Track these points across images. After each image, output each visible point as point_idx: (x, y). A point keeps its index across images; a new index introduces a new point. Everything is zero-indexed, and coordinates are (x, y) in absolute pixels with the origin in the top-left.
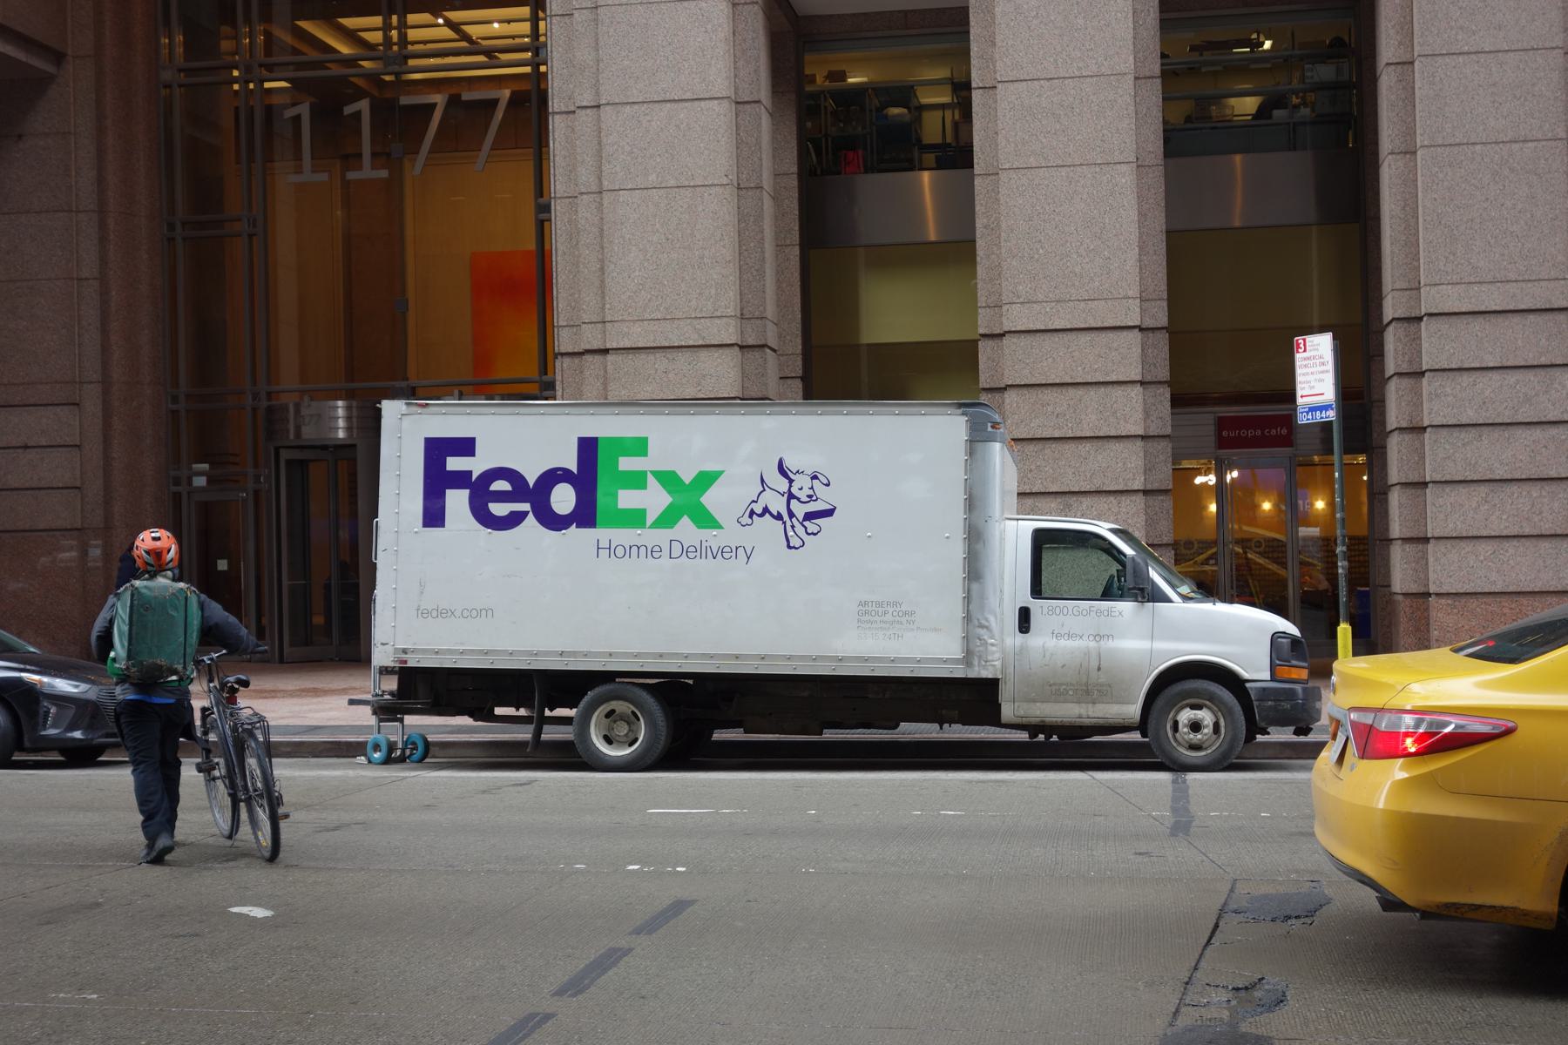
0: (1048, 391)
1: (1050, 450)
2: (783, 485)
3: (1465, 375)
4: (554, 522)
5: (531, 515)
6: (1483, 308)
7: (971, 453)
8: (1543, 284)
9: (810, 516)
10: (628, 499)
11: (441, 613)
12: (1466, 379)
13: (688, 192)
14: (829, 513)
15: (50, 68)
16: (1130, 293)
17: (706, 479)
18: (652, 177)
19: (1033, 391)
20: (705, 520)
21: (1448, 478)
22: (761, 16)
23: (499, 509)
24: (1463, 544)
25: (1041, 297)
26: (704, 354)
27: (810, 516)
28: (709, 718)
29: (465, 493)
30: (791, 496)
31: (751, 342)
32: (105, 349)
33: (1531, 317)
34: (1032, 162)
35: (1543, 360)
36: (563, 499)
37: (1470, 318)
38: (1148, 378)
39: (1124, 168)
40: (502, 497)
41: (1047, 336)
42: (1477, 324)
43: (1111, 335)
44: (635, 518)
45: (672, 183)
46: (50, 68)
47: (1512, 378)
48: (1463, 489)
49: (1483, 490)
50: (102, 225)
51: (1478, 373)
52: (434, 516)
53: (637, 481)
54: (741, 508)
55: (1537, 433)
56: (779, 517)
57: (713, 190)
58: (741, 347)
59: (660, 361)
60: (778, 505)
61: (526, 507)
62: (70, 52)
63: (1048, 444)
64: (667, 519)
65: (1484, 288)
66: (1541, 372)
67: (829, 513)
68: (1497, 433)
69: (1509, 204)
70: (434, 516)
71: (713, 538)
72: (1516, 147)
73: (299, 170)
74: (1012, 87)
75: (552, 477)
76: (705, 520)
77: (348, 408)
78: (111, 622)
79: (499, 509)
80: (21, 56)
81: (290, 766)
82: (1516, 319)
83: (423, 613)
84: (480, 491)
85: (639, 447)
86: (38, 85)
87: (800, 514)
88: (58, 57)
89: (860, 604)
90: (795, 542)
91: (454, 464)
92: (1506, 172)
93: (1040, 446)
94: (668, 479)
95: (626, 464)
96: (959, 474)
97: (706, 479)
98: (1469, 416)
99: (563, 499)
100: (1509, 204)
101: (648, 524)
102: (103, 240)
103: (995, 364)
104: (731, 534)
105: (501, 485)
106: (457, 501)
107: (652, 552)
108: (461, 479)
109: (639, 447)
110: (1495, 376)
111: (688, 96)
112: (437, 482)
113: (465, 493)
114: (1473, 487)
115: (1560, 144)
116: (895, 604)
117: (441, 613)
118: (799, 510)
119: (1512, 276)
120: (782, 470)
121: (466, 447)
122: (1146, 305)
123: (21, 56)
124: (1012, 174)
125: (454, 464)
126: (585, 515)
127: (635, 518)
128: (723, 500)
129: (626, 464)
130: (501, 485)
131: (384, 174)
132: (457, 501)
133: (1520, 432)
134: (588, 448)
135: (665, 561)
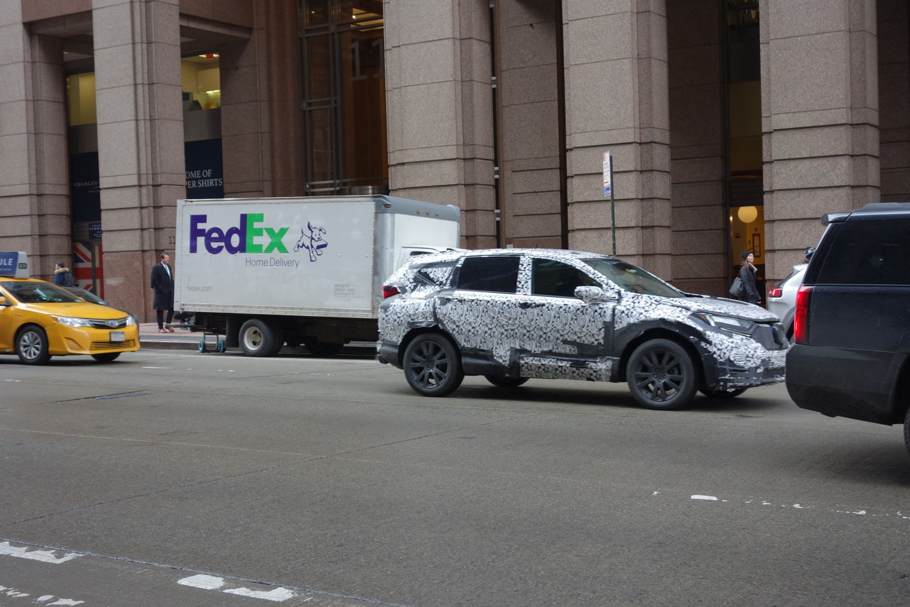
0: (591, 177)
1: (593, 207)
2: (309, 233)
3: (792, 162)
4: (232, 250)
5: (225, 249)
6: (801, 126)
7: (376, 218)
8: (832, 111)
9: (319, 247)
10: (257, 240)
11: (196, 289)
12: (792, 164)
13: (436, 85)
14: (325, 246)
15: (244, 35)
16: (630, 126)
17: (283, 231)
18: (422, 79)
19: (585, 177)
20: (283, 249)
21: (783, 218)
22: (179, 51)
23: (214, 245)
24: (790, 253)
25: (589, 129)
26: (443, 163)
27: (319, 247)
28: (297, 335)
29: (203, 238)
30: (312, 239)
31: (468, 157)
32: (273, 165)
33: (826, 129)
34: (585, 61)
35: (832, 153)
36: (235, 240)
37: (794, 131)
38: (644, 169)
39: (626, 61)
40: (215, 240)
41: (591, 149)
42: (799, 135)
43: (621, 147)
44: (258, 249)
45: (430, 81)
46: (244, 35)
47: (816, 163)
48: (790, 224)
49: (800, 223)
50: (271, 107)
51: (798, 161)
52: (193, 249)
53: (259, 232)
54: (294, 244)
55: (828, 192)
56: (308, 248)
57: (447, 84)
58: (464, 159)
59: (425, 168)
60: (307, 243)
61: (222, 244)
62: (255, 27)
63: (592, 204)
64: (270, 249)
65: (802, 115)
66: (831, 159)
67: (325, 246)
68: (807, 193)
69: (815, 68)
70: (193, 249)
71: (285, 257)
72: (819, 36)
73: (354, 75)
74: (575, 23)
75: (232, 231)
76: (283, 249)
77: (373, 189)
78: (600, 285)
79: (214, 245)
80: (226, 32)
81: (183, 353)
82: (818, 130)
83: (190, 289)
84: (207, 235)
85: (260, 218)
86: (243, 43)
87: (315, 247)
88: (250, 30)
89: (337, 286)
90: (313, 259)
91: (200, 226)
92: (814, 51)
93: (588, 205)
94: (270, 231)
95: (257, 225)
96: (371, 228)
97: (283, 231)
98: (794, 184)
99: (235, 240)
100: (815, 68)
101: (264, 249)
102: (271, 114)
103: (396, 178)
104: (290, 256)
105: (215, 235)
106: (201, 241)
107: (265, 263)
108: (202, 233)
109: (260, 218)
110: (807, 162)
111: (436, 38)
112: (195, 233)
113: (203, 238)
114: (795, 223)
115: (841, 33)
116: (348, 286)
117: (196, 289)
118: (315, 244)
119: (816, 108)
120: (309, 228)
121: (203, 219)
122: (642, 131)
123: (226, 32)
124: (576, 67)
125: (200, 226)
126: (242, 248)
127: (258, 249)
128: (288, 241)
129: (257, 225)
130: (215, 235)
131: (364, 77)
132: (201, 241)
133: (819, 192)
134: (244, 218)
135: (269, 267)
